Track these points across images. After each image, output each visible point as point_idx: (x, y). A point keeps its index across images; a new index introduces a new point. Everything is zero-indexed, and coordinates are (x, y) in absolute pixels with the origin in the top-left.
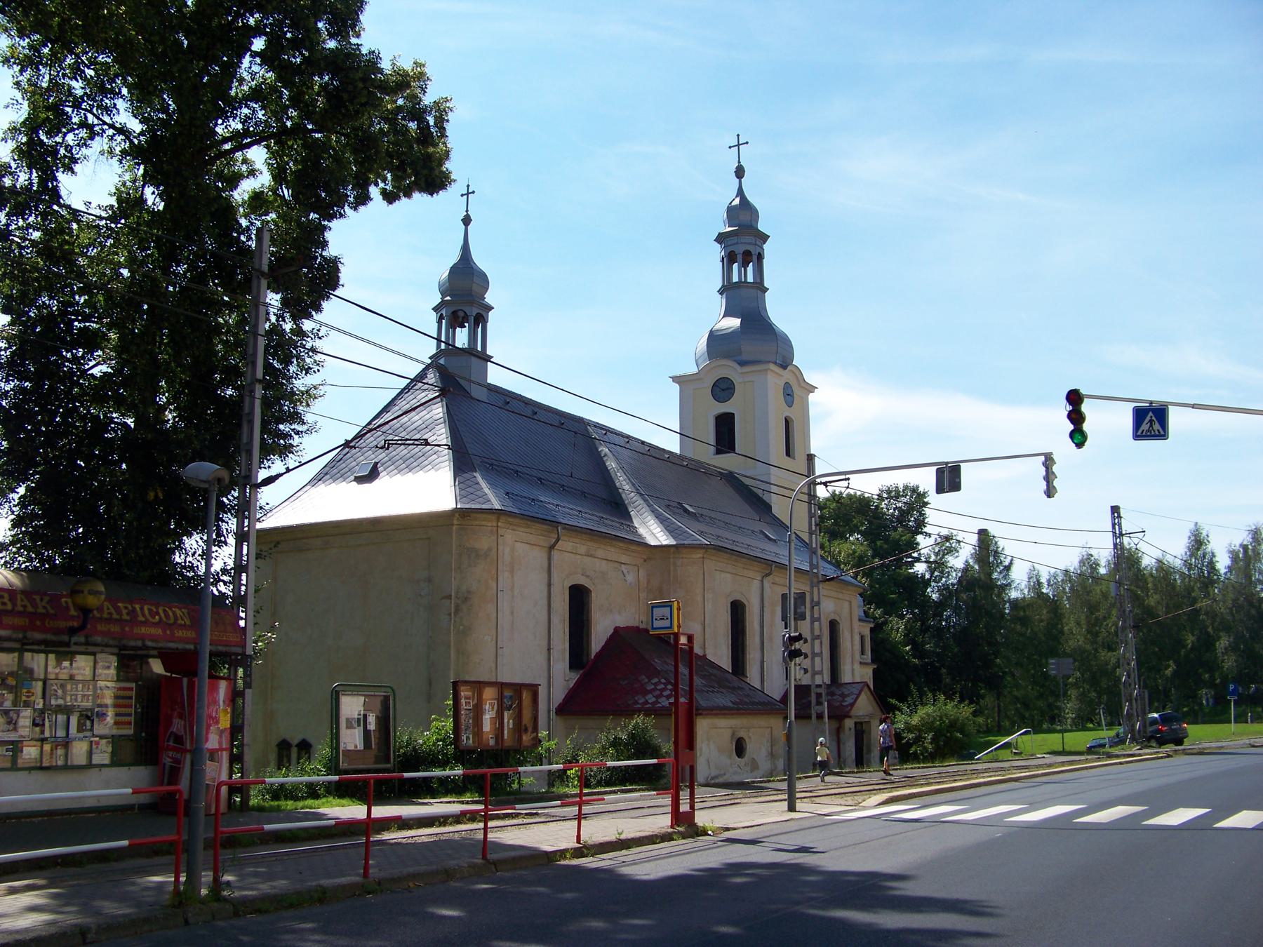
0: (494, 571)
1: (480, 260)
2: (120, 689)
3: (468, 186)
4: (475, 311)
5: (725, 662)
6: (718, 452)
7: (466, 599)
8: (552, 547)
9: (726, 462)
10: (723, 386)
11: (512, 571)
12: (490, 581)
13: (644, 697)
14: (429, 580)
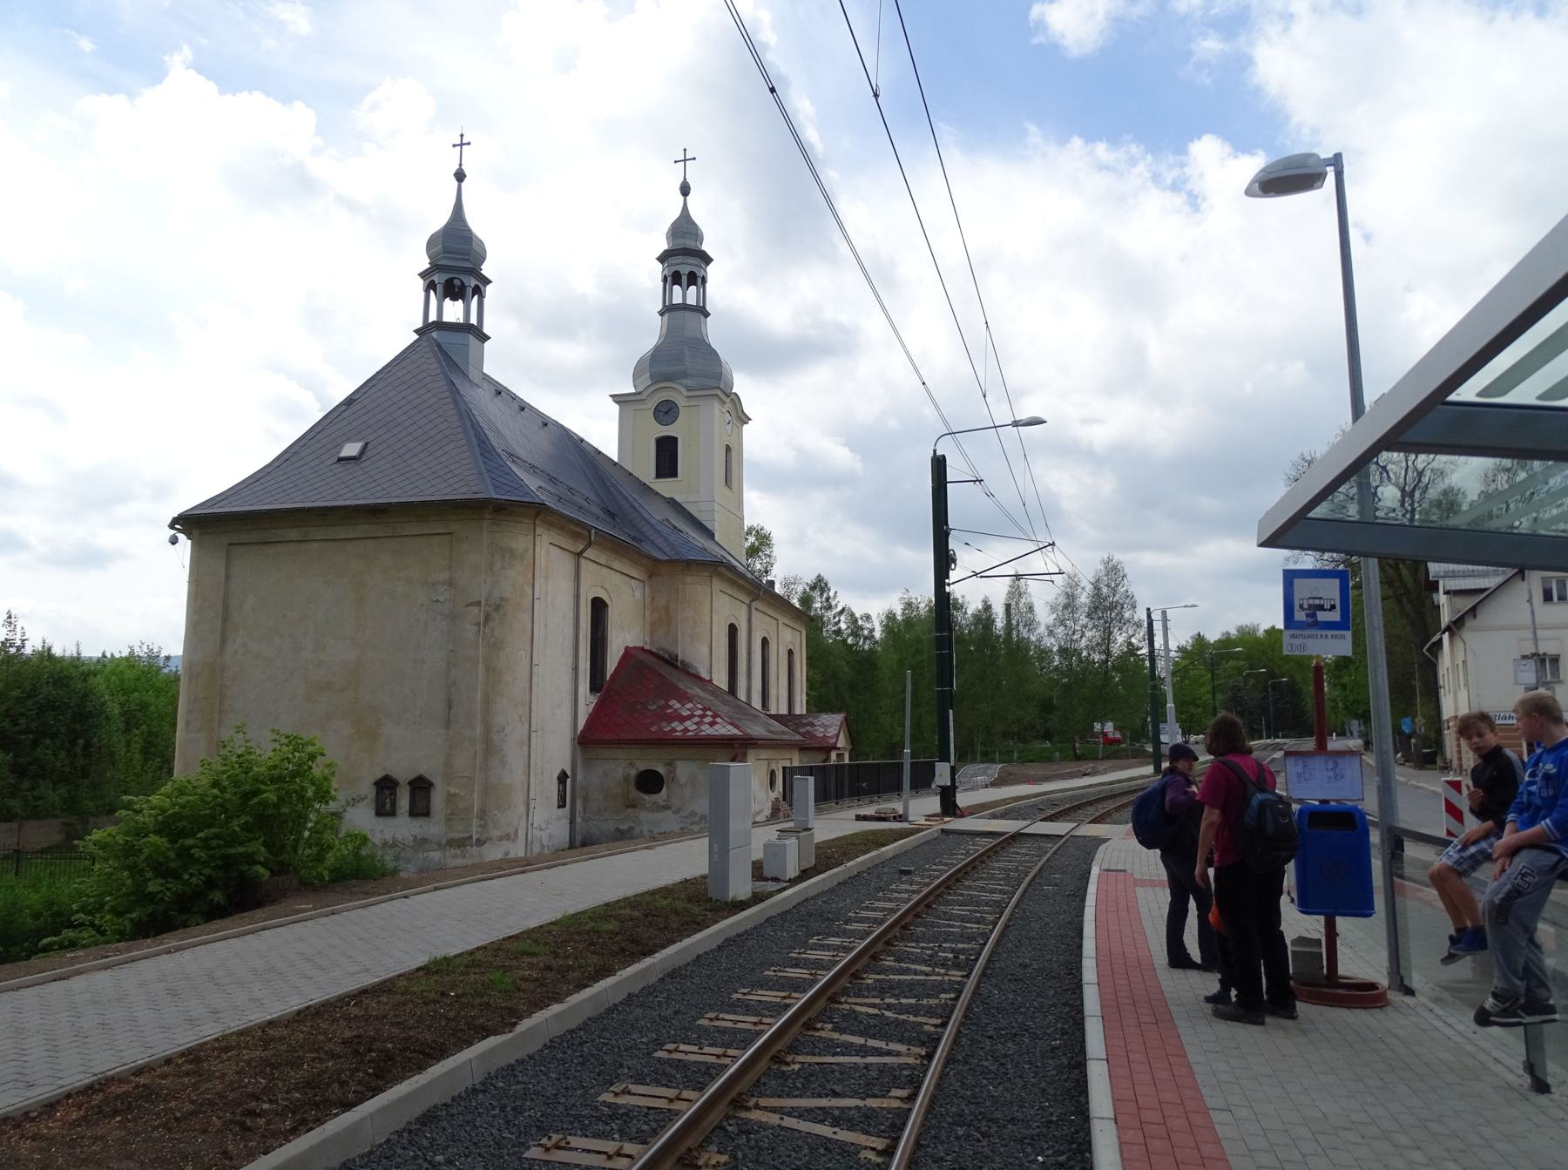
0: (530, 575)
1: (477, 223)
2: (1549, 828)
3: (462, 136)
4: (473, 282)
5: (724, 686)
6: (658, 476)
7: (498, 608)
8: (579, 554)
9: (665, 487)
10: (665, 409)
11: (546, 578)
12: (526, 588)
13: (681, 723)
14: (451, 583)
